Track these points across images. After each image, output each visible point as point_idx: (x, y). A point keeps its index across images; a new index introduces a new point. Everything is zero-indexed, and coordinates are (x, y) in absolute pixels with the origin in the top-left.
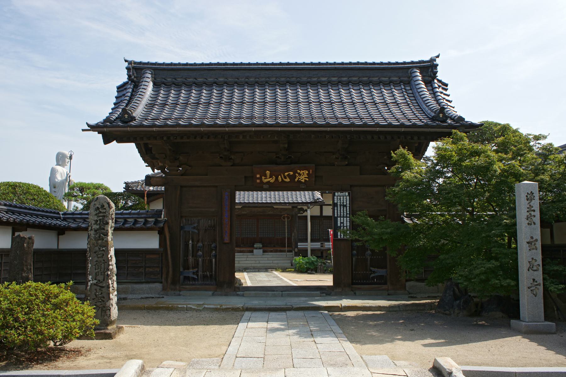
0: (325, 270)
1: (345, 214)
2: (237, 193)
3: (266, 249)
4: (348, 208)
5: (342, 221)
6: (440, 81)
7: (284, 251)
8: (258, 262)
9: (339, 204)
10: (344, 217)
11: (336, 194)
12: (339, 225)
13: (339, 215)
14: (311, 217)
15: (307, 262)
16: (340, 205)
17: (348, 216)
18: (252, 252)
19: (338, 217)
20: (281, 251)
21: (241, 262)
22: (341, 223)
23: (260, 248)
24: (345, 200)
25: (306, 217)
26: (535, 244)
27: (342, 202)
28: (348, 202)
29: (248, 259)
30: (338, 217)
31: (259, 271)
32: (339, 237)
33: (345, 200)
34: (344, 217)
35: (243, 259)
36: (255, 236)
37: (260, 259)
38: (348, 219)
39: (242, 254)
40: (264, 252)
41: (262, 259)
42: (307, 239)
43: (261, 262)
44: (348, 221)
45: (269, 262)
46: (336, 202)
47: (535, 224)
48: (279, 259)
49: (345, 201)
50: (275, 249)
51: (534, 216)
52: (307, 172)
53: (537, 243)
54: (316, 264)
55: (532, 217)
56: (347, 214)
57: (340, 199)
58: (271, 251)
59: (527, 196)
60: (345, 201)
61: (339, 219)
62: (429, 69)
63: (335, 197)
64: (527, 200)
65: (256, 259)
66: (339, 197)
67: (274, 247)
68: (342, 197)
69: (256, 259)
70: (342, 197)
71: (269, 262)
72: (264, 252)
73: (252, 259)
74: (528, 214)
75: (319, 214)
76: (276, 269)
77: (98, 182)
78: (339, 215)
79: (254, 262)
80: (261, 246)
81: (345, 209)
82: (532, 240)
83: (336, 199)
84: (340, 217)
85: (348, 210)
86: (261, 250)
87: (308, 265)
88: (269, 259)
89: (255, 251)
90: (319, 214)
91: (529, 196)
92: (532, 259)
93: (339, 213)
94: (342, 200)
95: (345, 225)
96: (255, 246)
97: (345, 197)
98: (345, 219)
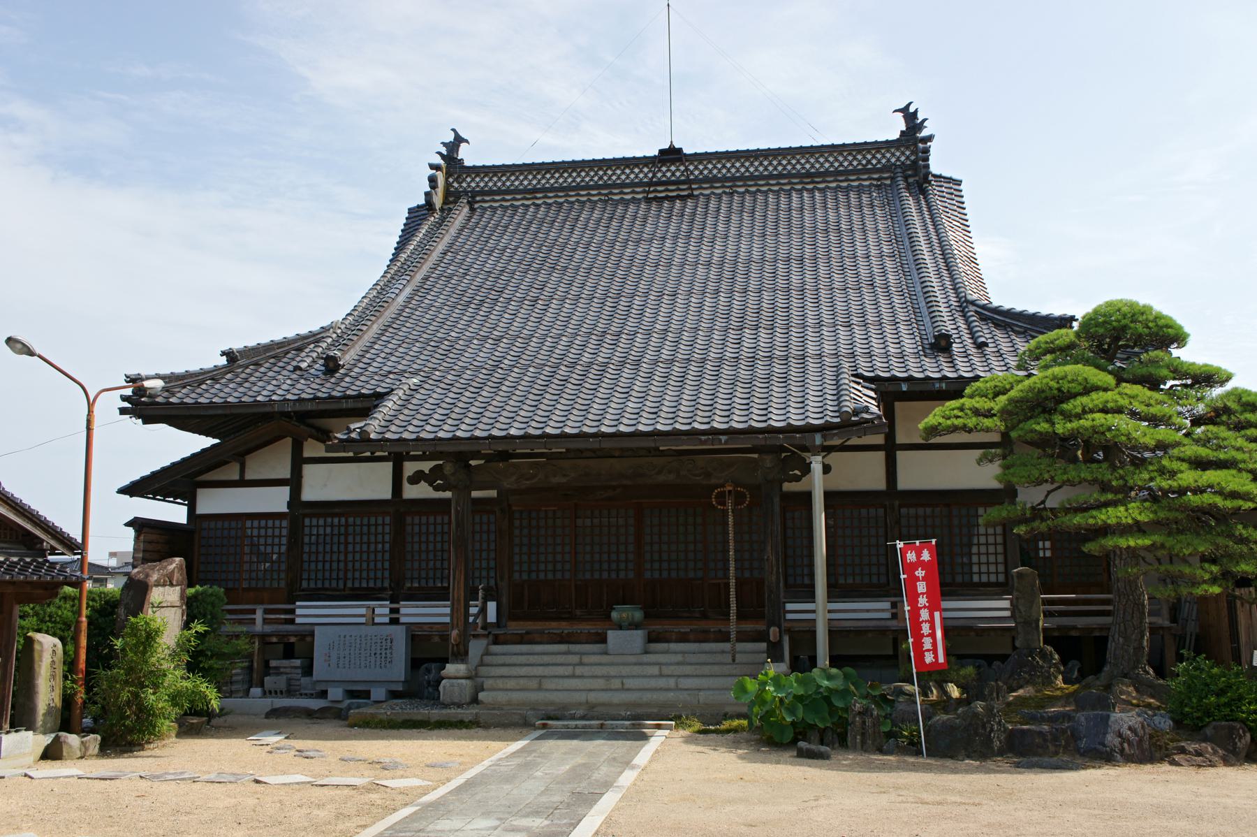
0: (890, 735)
2: (897, 404)
3: (657, 627)
6: (934, 176)
7: (725, 637)
8: (616, 683)
14: (828, 495)
15: (799, 698)
18: (603, 640)
20: (703, 637)
21: (548, 684)
23: (634, 626)
25: (807, 497)
29: (579, 670)
35: (560, 670)
36: (631, 575)
37: (625, 670)
39: (563, 647)
40: (652, 638)
41: (637, 670)
42: (812, 587)
43: (629, 683)
45: (662, 683)
48: (706, 670)
50: (703, 625)
54: (839, 703)
58: (683, 638)
62: (901, 169)
65: (612, 671)
67: (704, 616)
69: (612, 671)
71: (662, 683)
72: (652, 638)
73: (598, 671)
75: (880, 484)
76: (677, 718)
77: (1165, 312)
79: (600, 683)
80: (638, 615)
86: (638, 636)
87: (800, 713)
88: (666, 670)
89: (611, 634)
90: (880, 484)
96: (614, 615)
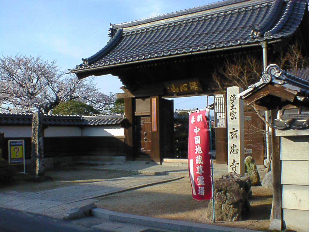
1: (222, 110)
4: (224, 106)
5: (220, 115)
9: (218, 103)
10: (221, 112)
11: (216, 96)
12: (218, 118)
13: (218, 111)
16: (219, 104)
17: (224, 111)
19: (217, 112)
22: (219, 117)
24: (221, 100)
26: (236, 134)
27: (220, 102)
28: (223, 102)
30: (217, 112)
31: (160, 151)
32: (218, 126)
33: (221, 100)
34: (221, 112)
38: (224, 113)
44: (224, 115)
46: (216, 102)
47: (236, 118)
49: (221, 101)
51: (236, 113)
52: (195, 83)
53: (237, 133)
55: (234, 114)
56: (223, 110)
57: (218, 100)
59: (231, 98)
60: (221, 101)
61: (218, 114)
63: (216, 99)
64: (231, 100)
66: (218, 99)
68: (219, 99)
70: (219, 99)
74: (231, 111)
78: (218, 111)
81: (222, 107)
82: (234, 131)
83: (216, 100)
84: (219, 112)
85: (224, 107)
91: (232, 98)
92: (234, 145)
93: (218, 110)
94: (219, 100)
95: (222, 118)
97: (221, 98)
98: (222, 113)
